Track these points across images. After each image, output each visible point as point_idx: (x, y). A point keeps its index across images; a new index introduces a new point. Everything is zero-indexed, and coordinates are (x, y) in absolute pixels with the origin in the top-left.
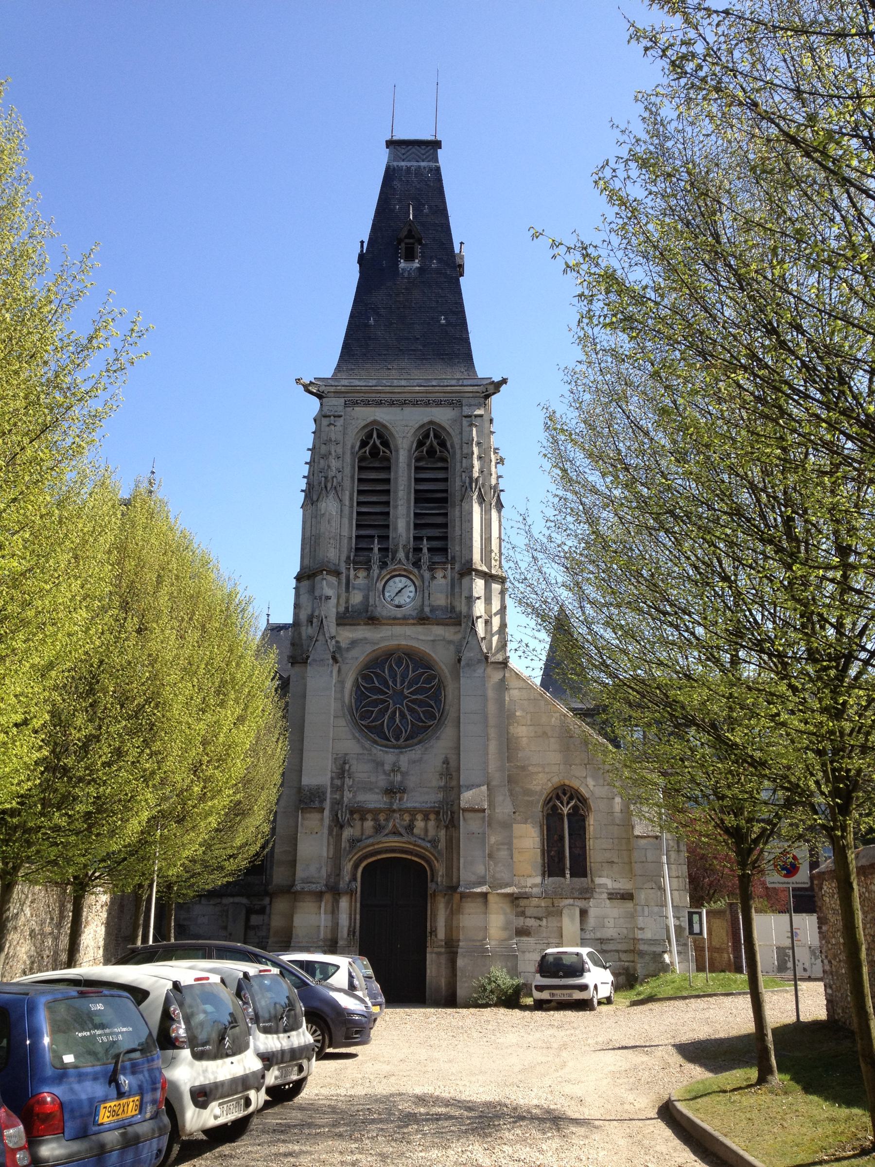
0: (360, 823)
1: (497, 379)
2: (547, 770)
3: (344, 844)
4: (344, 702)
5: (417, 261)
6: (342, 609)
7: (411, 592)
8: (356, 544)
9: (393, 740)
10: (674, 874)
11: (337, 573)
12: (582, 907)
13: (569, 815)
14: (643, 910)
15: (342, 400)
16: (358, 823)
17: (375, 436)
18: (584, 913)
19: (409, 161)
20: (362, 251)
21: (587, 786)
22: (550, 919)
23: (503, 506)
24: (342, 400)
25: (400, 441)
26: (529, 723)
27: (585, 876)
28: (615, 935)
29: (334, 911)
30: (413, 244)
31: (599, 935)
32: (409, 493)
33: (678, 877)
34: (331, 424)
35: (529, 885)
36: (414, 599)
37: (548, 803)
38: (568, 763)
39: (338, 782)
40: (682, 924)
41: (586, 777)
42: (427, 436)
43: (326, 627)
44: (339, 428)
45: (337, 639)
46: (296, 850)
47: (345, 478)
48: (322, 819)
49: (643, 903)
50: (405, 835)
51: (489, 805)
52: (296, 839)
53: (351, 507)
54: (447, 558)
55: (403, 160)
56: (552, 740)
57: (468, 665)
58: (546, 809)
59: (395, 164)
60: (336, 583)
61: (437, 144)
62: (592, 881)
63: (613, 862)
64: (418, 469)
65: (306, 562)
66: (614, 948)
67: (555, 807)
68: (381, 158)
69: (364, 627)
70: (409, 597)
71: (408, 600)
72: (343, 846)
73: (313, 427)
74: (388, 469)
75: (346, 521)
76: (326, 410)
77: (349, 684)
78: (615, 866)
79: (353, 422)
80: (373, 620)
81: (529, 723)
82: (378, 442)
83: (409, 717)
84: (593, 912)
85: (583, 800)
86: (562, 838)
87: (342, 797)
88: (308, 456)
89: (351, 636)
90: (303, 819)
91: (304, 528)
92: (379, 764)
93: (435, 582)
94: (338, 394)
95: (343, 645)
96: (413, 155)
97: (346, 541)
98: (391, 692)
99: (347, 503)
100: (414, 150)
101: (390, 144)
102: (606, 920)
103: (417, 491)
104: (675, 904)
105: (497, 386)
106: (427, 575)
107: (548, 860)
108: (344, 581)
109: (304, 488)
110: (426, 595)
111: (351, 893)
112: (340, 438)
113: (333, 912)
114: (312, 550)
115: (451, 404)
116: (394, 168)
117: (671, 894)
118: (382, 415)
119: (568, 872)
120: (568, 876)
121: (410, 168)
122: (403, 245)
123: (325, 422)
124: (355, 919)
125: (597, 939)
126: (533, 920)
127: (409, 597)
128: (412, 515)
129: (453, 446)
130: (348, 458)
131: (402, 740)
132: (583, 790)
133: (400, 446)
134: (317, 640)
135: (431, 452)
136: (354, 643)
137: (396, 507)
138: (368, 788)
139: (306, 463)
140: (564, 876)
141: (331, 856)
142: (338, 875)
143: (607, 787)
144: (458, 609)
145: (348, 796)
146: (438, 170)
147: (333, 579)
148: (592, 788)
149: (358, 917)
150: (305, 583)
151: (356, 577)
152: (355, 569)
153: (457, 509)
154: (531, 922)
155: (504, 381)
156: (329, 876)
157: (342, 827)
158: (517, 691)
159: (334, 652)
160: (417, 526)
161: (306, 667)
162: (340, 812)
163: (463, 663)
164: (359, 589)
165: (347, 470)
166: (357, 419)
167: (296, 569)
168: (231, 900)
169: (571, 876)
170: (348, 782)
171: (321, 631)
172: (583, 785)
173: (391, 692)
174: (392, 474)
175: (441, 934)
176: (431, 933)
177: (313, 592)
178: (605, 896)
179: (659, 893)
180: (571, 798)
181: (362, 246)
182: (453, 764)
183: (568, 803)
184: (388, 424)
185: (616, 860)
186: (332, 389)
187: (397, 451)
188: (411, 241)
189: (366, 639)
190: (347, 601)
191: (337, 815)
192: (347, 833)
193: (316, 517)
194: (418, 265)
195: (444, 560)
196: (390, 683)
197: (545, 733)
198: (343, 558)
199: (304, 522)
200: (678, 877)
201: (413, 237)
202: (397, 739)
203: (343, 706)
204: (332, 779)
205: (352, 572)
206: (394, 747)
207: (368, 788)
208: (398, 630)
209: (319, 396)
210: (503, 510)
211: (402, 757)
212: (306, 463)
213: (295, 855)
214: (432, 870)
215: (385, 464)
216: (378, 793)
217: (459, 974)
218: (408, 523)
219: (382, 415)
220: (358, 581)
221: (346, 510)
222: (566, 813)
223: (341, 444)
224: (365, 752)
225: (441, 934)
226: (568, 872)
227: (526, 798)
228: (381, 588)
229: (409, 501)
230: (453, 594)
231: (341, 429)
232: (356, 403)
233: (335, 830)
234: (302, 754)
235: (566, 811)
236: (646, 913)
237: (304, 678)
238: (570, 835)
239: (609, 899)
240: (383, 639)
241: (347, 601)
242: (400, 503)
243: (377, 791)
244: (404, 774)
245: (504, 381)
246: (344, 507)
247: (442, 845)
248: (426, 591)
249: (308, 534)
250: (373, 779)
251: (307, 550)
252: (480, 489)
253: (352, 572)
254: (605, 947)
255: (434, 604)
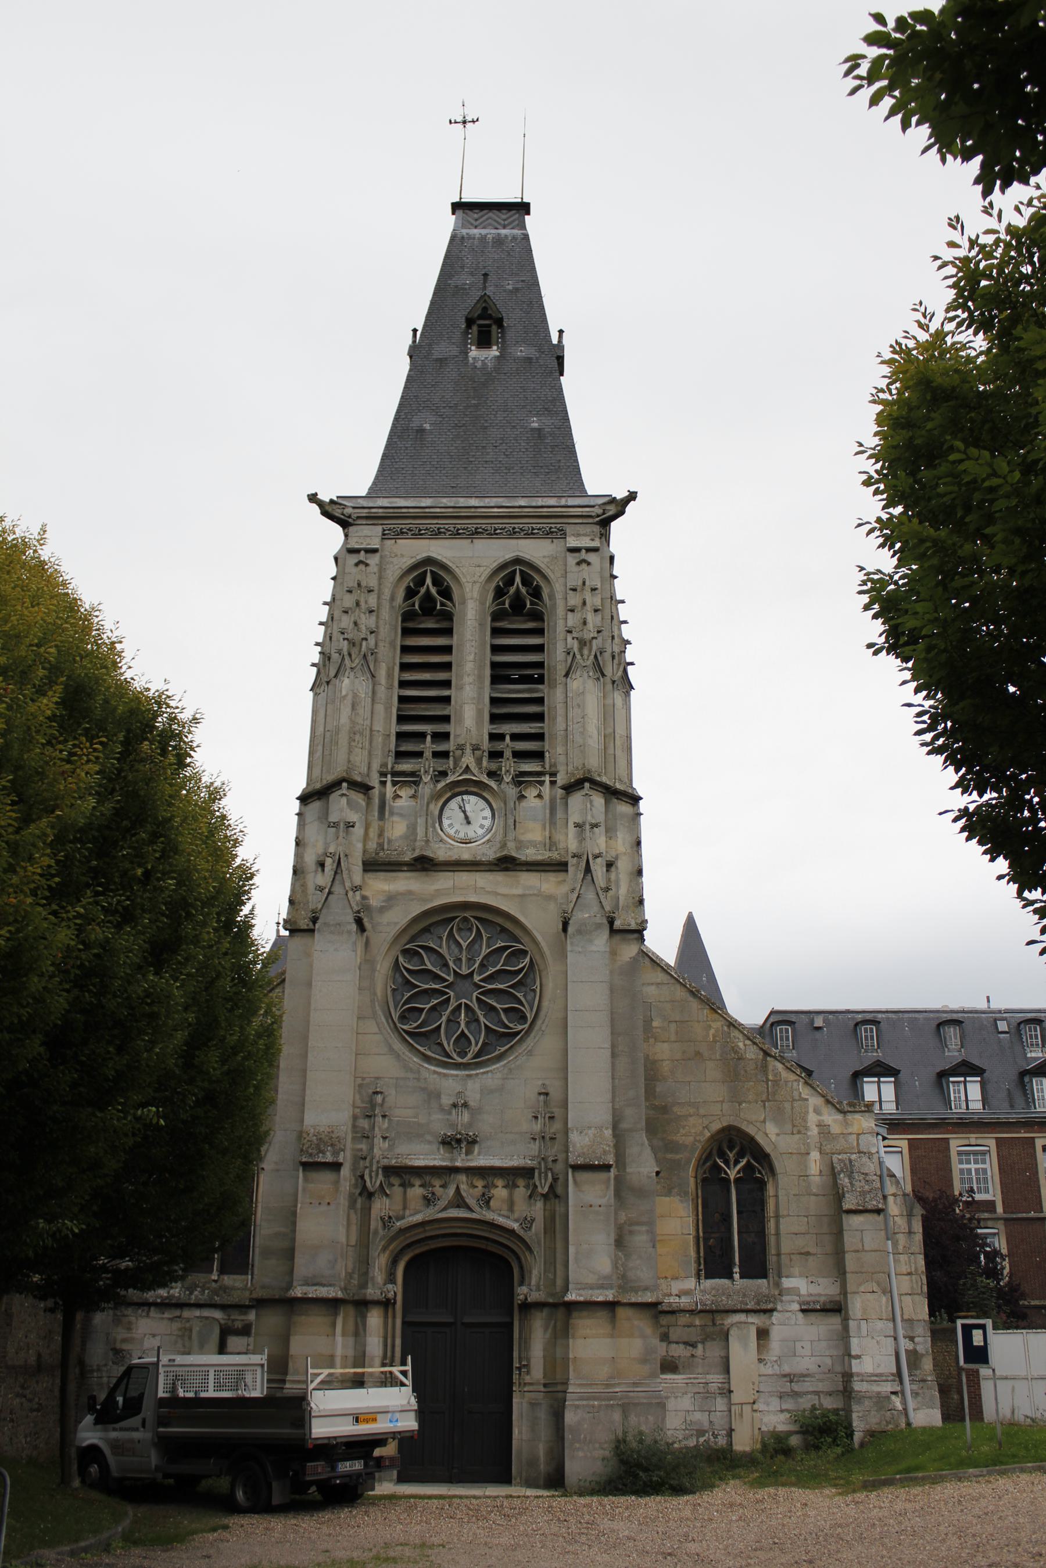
0: (401, 1189)
1: (620, 494)
2: (702, 1111)
3: (375, 1224)
4: (375, 994)
5: (495, 348)
6: (372, 845)
7: (485, 818)
8: (397, 746)
9: (455, 1056)
10: (904, 1269)
11: (364, 788)
12: (760, 1324)
13: (737, 1180)
14: (859, 1327)
15: (379, 529)
16: (397, 1190)
17: (429, 581)
18: (763, 1334)
19: (484, 228)
20: (414, 341)
21: (767, 1135)
22: (708, 1344)
23: (632, 688)
24: (379, 529)
25: (468, 587)
26: (673, 1038)
27: (764, 1275)
28: (813, 1368)
29: (359, 1332)
30: (490, 326)
31: (787, 1369)
32: (481, 668)
33: (909, 1274)
34: (360, 562)
35: (674, 1291)
36: (489, 830)
37: (704, 1163)
38: (736, 1098)
39: (364, 1123)
40: (918, 1348)
41: (764, 1122)
42: (509, 581)
43: (345, 873)
44: (373, 568)
45: (364, 893)
46: (294, 1231)
47: (381, 644)
48: (337, 1182)
49: (859, 1315)
50: (477, 1208)
51: (617, 1162)
52: (294, 1214)
53: (390, 687)
54: (543, 766)
55: (476, 227)
56: (710, 1065)
57: (579, 932)
58: (700, 1171)
59: (464, 232)
60: (364, 804)
61: (524, 208)
62: (778, 1285)
63: (808, 1254)
64: (496, 632)
65: (317, 772)
66: (811, 1389)
67: (716, 1168)
68: (447, 223)
69: (408, 874)
70: (482, 826)
71: (480, 832)
72: (372, 1227)
73: (333, 571)
74: (449, 632)
75: (380, 708)
76: (353, 544)
77: (383, 967)
78: (811, 1258)
79: (395, 560)
80: (424, 864)
81: (673, 1038)
82: (433, 591)
83: (482, 1019)
84: (777, 1333)
85: (762, 1157)
86: (727, 1219)
87: (372, 1148)
88: (323, 614)
89: (386, 887)
90: (306, 1180)
91: (314, 722)
92: (434, 1095)
93: (524, 804)
94: (372, 518)
95: (374, 902)
96: (490, 221)
97: (380, 740)
98: (451, 979)
99: (383, 681)
100: (490, 214)
101: (456, 207)
102: (798, 1345)
103: (494, 665)
104: (906, 1317)
105: (618, 507)
106: (512, 791)
107: (705, 1253)
108: (376, 801)
109: (316, 661)
110: (511, 822)
111: (386, 1304)
112: (373, 583)
113: (356, 1334)
114: (327, 753)
115: (549, 534)
116: (463, 238)
117: (901, 1301)
118: (441, 550)
119: (736, 1269)
120: (737, 1276)
121: (486, 236)
122: (475, 328)
123: (353, 559)
124: (393, 1346)
125: (785, 1376)
126: (682, 1346)
127: (482, 826)
128: (487, 700)
129: (552, 596)
130: (385, 613)
131: (470, 1056)
132: (760, 1139)
133: (468, 595)
134: (330, 893)
135: (518, 605)
136: (391, 899)
137: (460, 688)
138: (414, 1133)
139: (321, 624)
140: (730, 1276)
141: (353, 1243)
142: (366, 1273)
143: (797, 1136)
144: (562, 845)
145: (380, 1146)
146: (526, 237)
147: (359, 798)
148: (773, 1138)
149: (398, 1342)
150: (316, 806)
151: (397, 797)
152: (394, 783)
153: (559, 692)
154: (678, 1351)
155: (632, 496)
156: (350, 1276)
157: (370, 1195)
158: (653, 987)
159: (358, 912)
160: (494, 718)
161: (314, 936)
162: (367, 1172)
163: (571, 929)
164: (401, 815)
165: (384, 631)
166: (402, 556)
167: (300, 785)
168: (197, 1313)
169: (741, 1277)
170: (382, 1124)
171: (338, 877)
172: (761, 1133)
173: (451, 979)
174: (455, 637)
175: (537, 1372)
176: (519, 1369)
177: (327, 819)
178: (796, 1307)
179: (884, 1299)
180: (741, 1155)
181: (415, 335)
182: (555, 1094)
183: (736, 1162)
184: (448, 563)
185: (812, 1250)
186: (364, 512)
187: (464, 602)
188: (487, 322)
189: (410, 893)
190: (381, 834)
191: (362, 1177)
192: (380, 1207)
193: (333, 702)
194: (497, 353)
195: (539, 769)
196: (451, 964)
197: (698, 1054)
198: (376, 766)
199: (315, 712)
200: (909, 1274)
201: (490, 317)
202: (463, 1054)
203: (372, 1001)
204: (355, 1118)
205: (389, 789)
206: (458, 1066)
207: (414, 1133)
208: (464, 878)
209: (344, 523)
210: (632, 693)
211: (470, 1084)
212: (321, 624)
213: (293, 1240)
214: (521, 1268)
215: (444, 625)
216: (430, 1142)
217: (568, 1436)
218: (480, 712)
219: (441, 550)
220: (399, 803)
221: (382, 691)
222: (732, 1177)
223: (376, 592)
224: (410, 1075)
225: (537, 1372)
226: (736, 1269)
227: (669, 1156)
228: (437, 813)
229: (480, 678)
230: (553, 822)
231: (376, 569)
232: (401, 534)
233: (359, 1200)
234: (305, 1076)
235: (732, 1174)
236: (864, 1332)
237: (308, 955)
238: (738, 1212)
239: (803, 1311)
240: (438, 893)
241: (381, 834)
242: (467, 680)
243: (428, 1137)
244: (475, 1112)
245: (632, 496)
246: (378, 687)
247: (538, 1226)
248: (509, 816)
249: (320, 730)
250: (422, 1119)
251: (319, 754)
252: (596, 656)
253: (389, 789)
254: (796, 1387)
255: (522, 838)
